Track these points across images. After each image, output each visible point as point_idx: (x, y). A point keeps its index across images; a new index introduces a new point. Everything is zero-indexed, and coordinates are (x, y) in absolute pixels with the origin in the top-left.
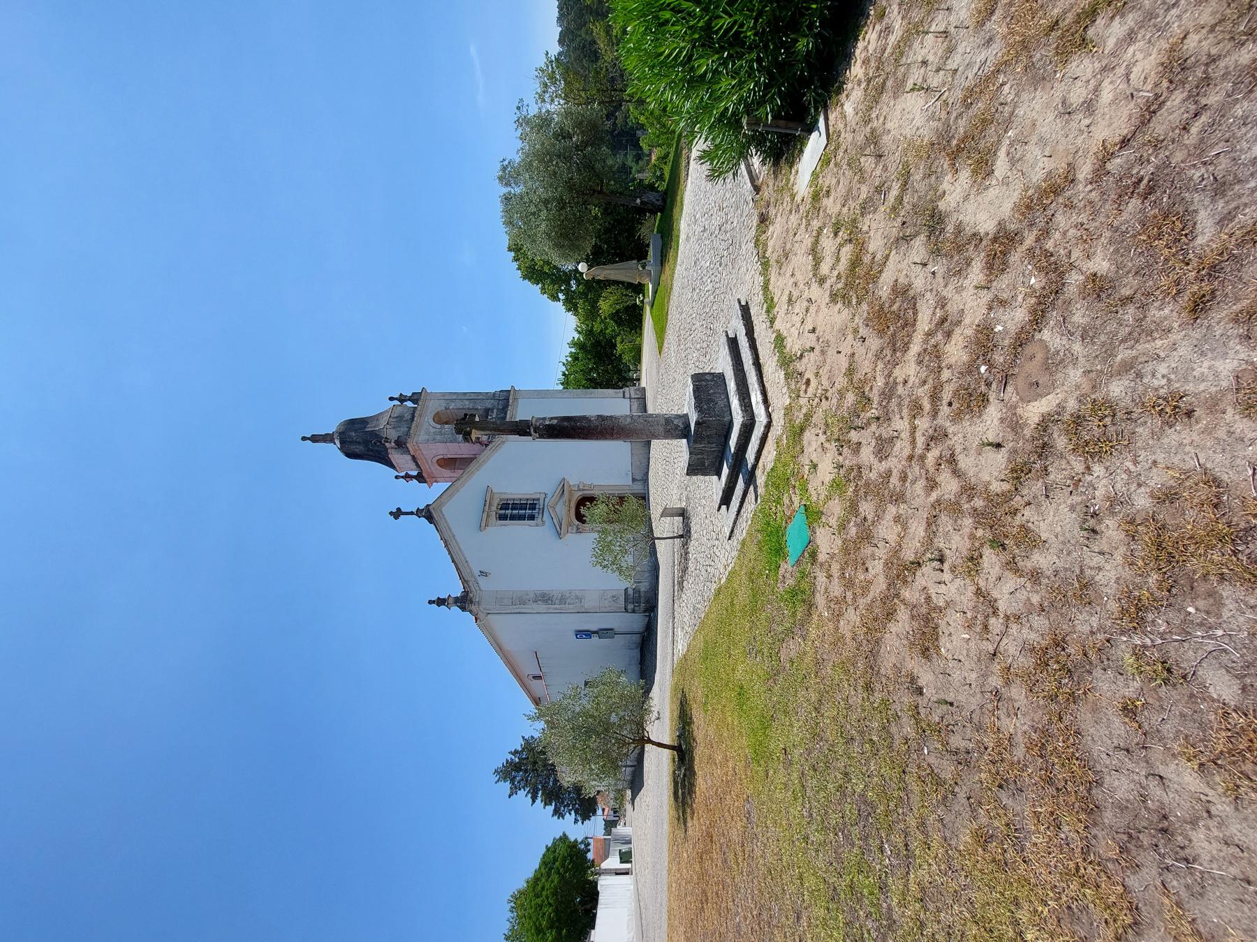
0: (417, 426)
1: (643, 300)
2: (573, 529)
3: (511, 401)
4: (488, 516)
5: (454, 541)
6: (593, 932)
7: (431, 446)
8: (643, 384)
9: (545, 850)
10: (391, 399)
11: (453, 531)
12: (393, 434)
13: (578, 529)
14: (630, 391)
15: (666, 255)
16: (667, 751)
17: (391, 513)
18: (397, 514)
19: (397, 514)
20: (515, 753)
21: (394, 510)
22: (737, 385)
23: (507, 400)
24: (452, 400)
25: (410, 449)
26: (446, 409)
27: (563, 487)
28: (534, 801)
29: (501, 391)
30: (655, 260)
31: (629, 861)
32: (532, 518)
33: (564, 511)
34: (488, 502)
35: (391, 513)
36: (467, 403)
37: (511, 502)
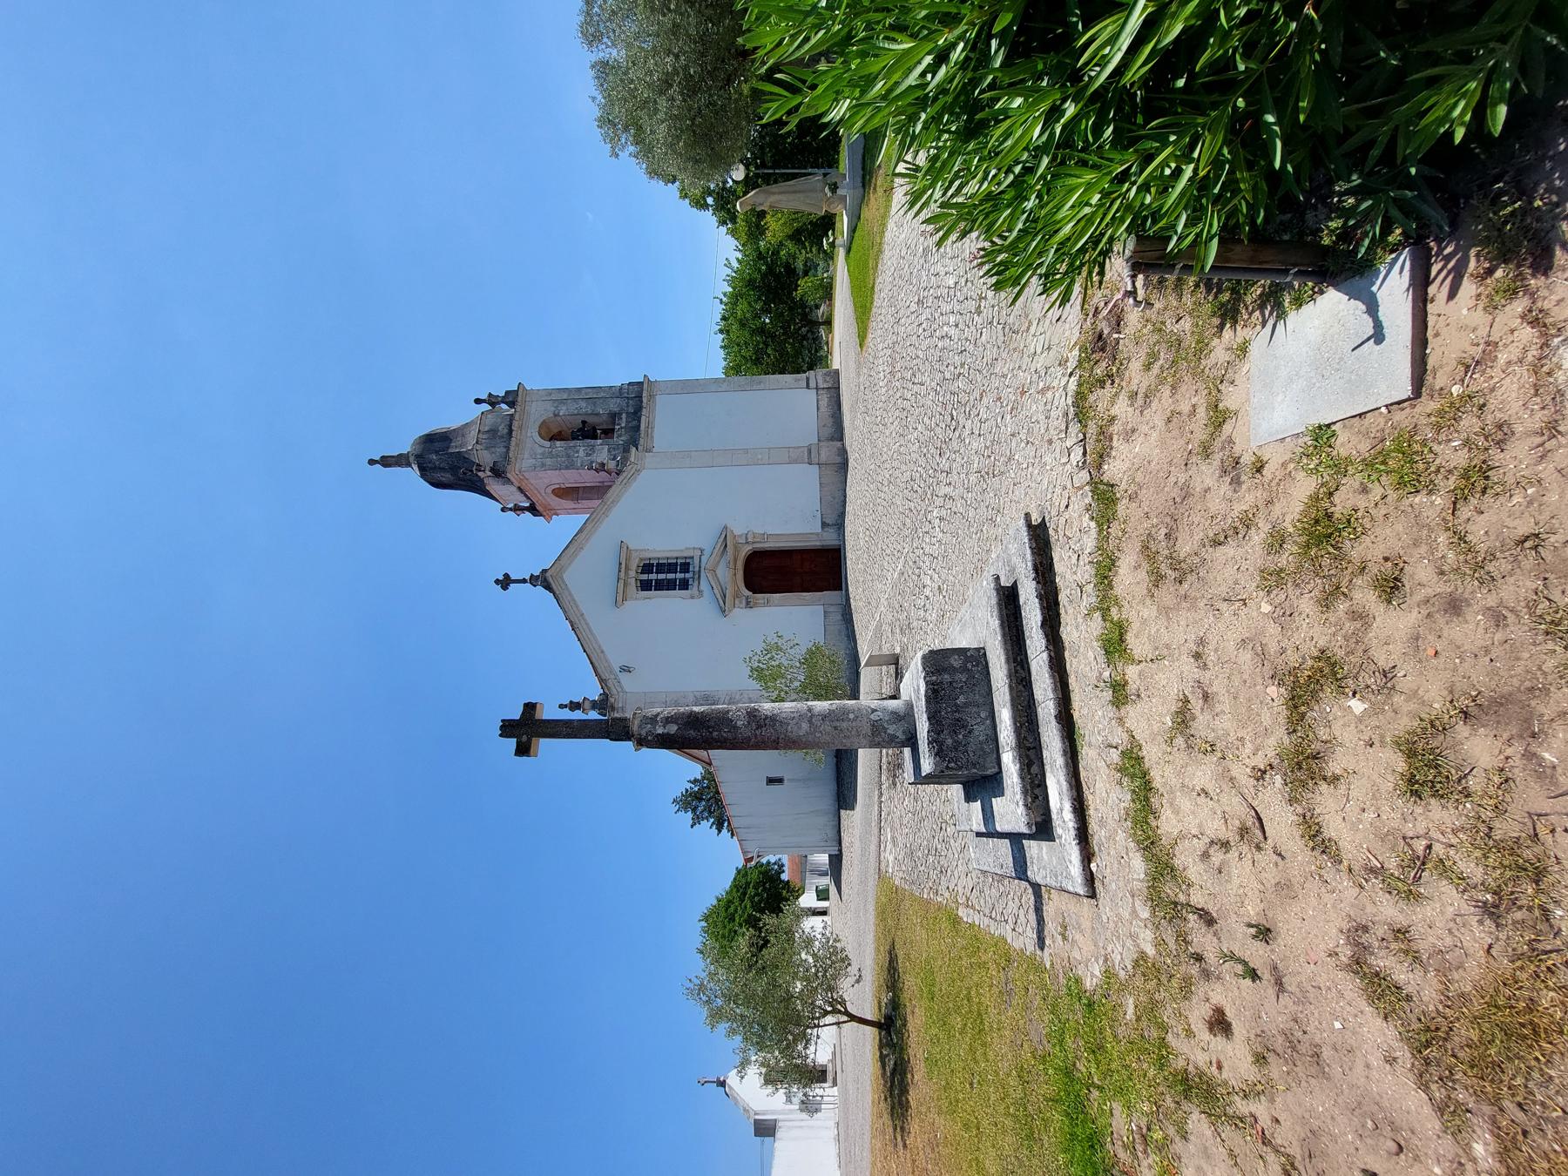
0: (517, 445)
1: (834, 241)
2: (741, 602)
3: (645, 400)
4: (625, 585)
5: (582, 621)
7: (541, 474)
8: (836, 365)
9: (735, 872)
10: (478, 401)
11: (581, 607)
12: (486, 458)
13: (748, 603)
14: (816, 376)
15: (870, 181)
16: (868, 1028)
17: (497, 582)
18: (505, 582)
19: (505, 582)
20: (695, 781)
21: (501, 578)
22: (1018, 731)
23: (640, 397)
24: (563, 402)
25: (512, 479)
26: (555, 415)
27: (725, 540)
28: (720, 831)
30: (853, 178)
31: (827, 899)
32: (684, 585)
33: (729, 575)
34: (623, 566)
35: (497, 582)
36: (583, 404)
37: (655, 562)
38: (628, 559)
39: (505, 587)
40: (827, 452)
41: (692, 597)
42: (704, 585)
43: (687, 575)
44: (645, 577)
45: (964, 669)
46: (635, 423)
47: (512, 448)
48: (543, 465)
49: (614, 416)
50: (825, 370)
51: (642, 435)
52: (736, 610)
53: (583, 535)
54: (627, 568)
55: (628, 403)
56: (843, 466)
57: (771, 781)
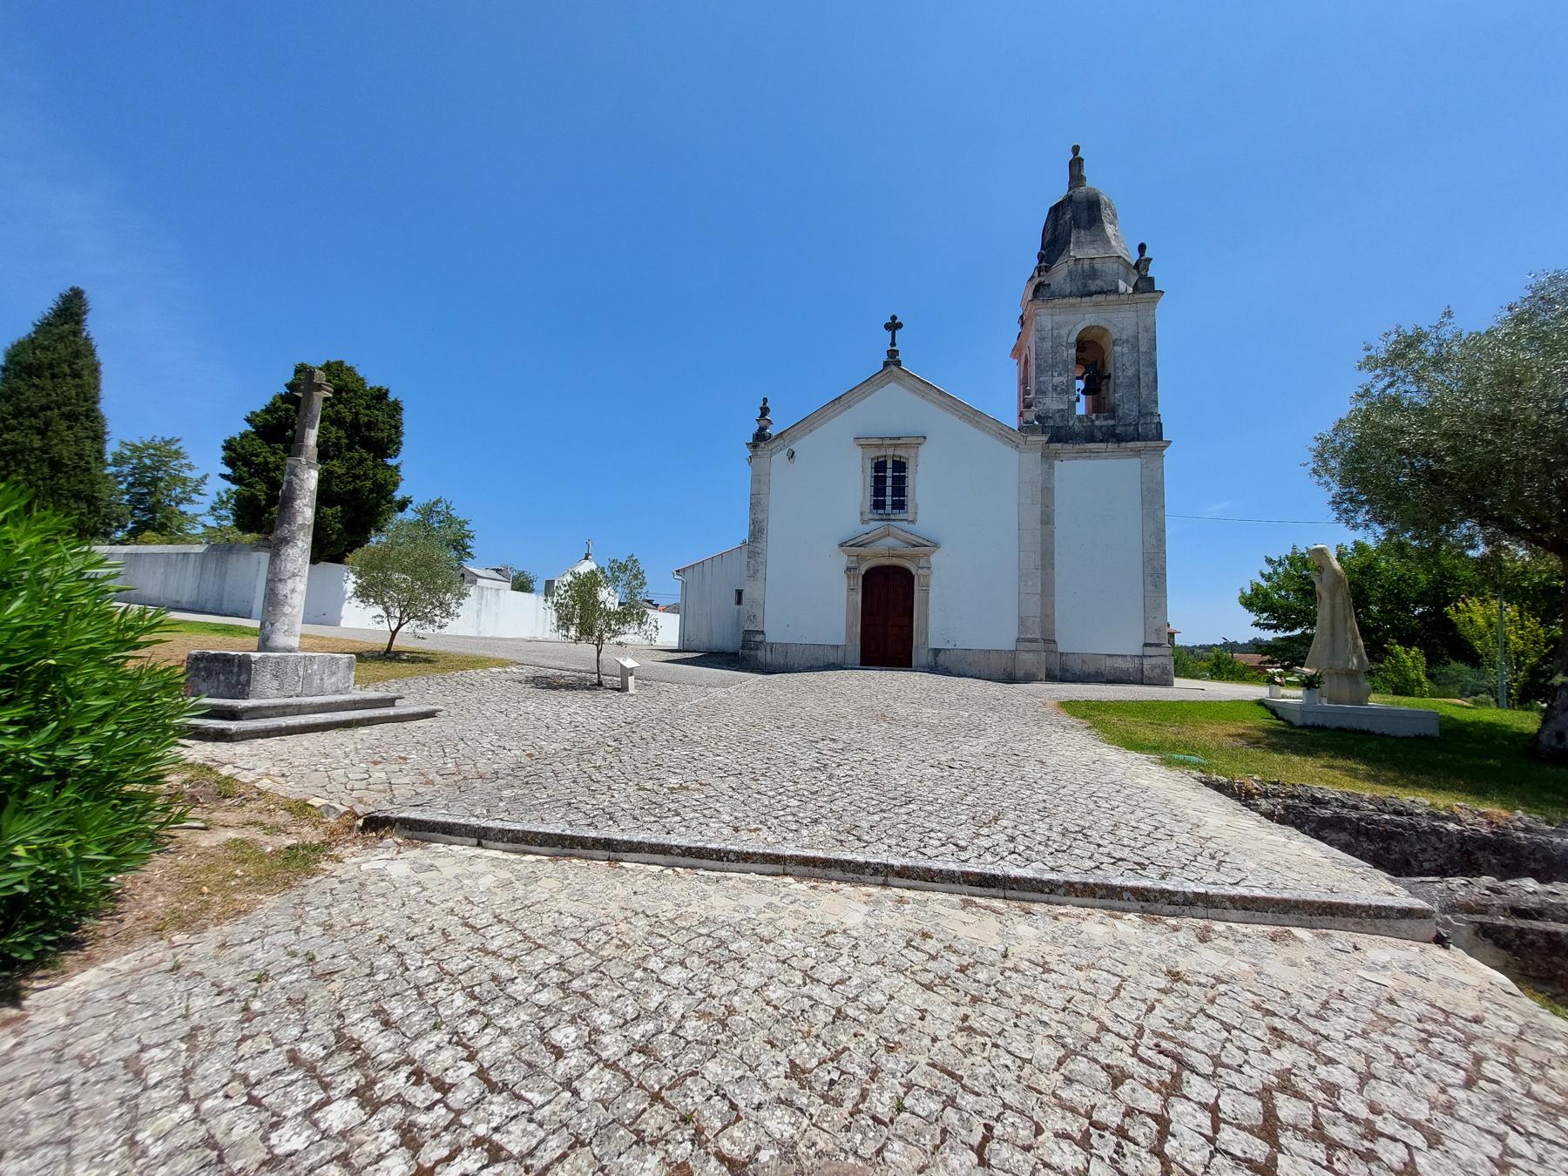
0: (1072, 305)
1: (1276, 683)
3: (1130, 445)
4: (877, 446)
6: (1240, 642)
10: (1142, 248)
16: (388, 641)
17: (894, 318)
19: (893, 326)
24: (1135, 347)
29: (1160, 425)
32: (878, 505)
33: (886, 548)
35: (894, 318)
38: (906, 446)
39: (887, 327)
40: (1031, 660)
41: (862, 514)
42: (874, 525)
43: (888, 508)
44: (889, 464)
45: (238, 683)
46: (1099, 435)
47: (1065, 301)
48: (1043, 339)
49: (1112, 412)
50: (1171, 668)
51: (1077, 446)
52: (845, 557)
53: (938, 396)
54: (895, 446)
55: (1130, 424)
56: (1010, 678)
57: (739, 593)
